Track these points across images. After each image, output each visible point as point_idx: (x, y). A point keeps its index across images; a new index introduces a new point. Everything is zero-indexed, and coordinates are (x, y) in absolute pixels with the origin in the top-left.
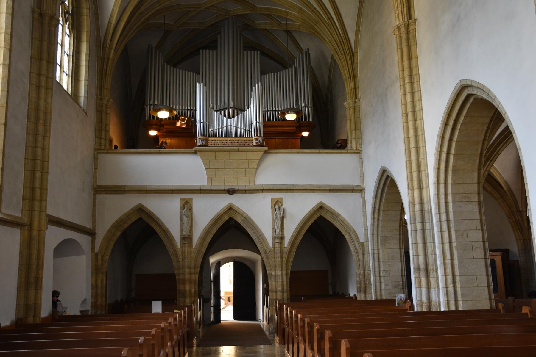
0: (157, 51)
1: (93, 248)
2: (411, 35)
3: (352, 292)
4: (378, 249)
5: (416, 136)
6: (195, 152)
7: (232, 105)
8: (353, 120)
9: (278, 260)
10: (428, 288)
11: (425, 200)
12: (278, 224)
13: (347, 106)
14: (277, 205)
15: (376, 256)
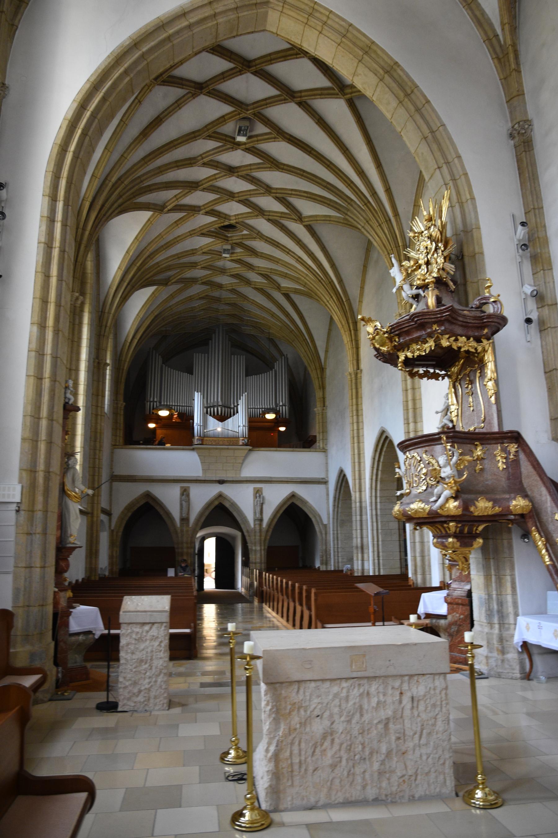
0: (154, 351)
1: (110, 526)
2: (359, 380)
3: (317, 564)
4: (337, 530)
5: (359, 454)
6: (193, 449)
7: (220, 403)
8: (321, 424)
9: (258, 538)
10: (363, 560)
11: (363, 500)
12: (258, 509)
13: (317, 412)
14: (258, 493)
15: (335, 535)
